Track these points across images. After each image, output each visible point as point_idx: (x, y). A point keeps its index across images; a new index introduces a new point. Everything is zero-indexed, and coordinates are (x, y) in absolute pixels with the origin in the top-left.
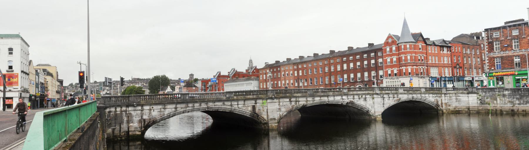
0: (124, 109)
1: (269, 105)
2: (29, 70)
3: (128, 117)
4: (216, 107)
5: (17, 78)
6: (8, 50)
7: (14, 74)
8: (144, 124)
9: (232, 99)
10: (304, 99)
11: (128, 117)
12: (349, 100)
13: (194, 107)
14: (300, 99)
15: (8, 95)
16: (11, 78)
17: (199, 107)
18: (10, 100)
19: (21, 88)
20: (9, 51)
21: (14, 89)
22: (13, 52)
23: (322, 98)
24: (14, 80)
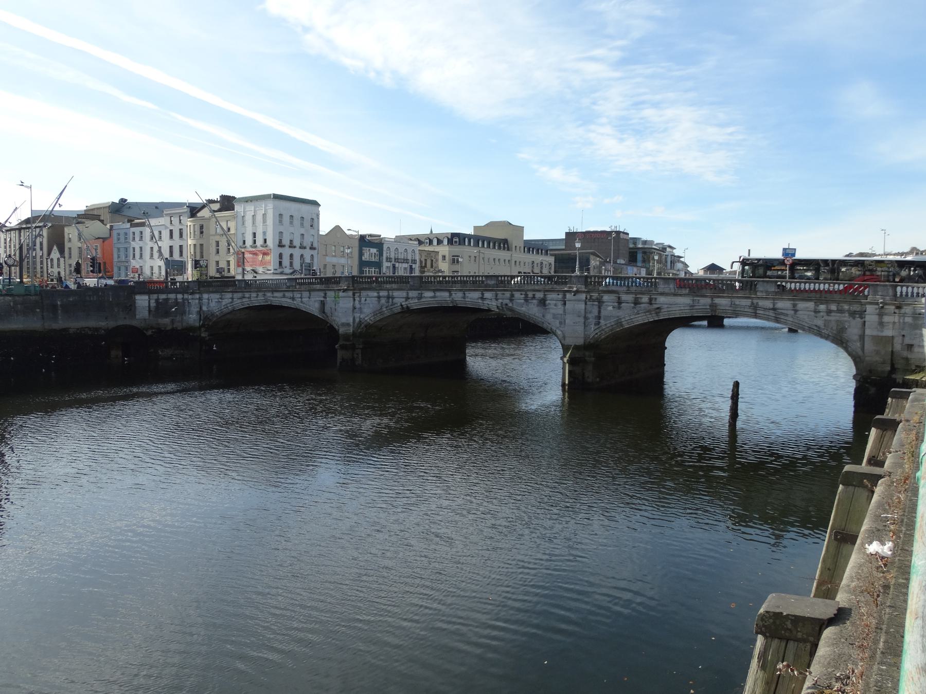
10: (404, 294)
14: (396, 294)
23: (438, 294)
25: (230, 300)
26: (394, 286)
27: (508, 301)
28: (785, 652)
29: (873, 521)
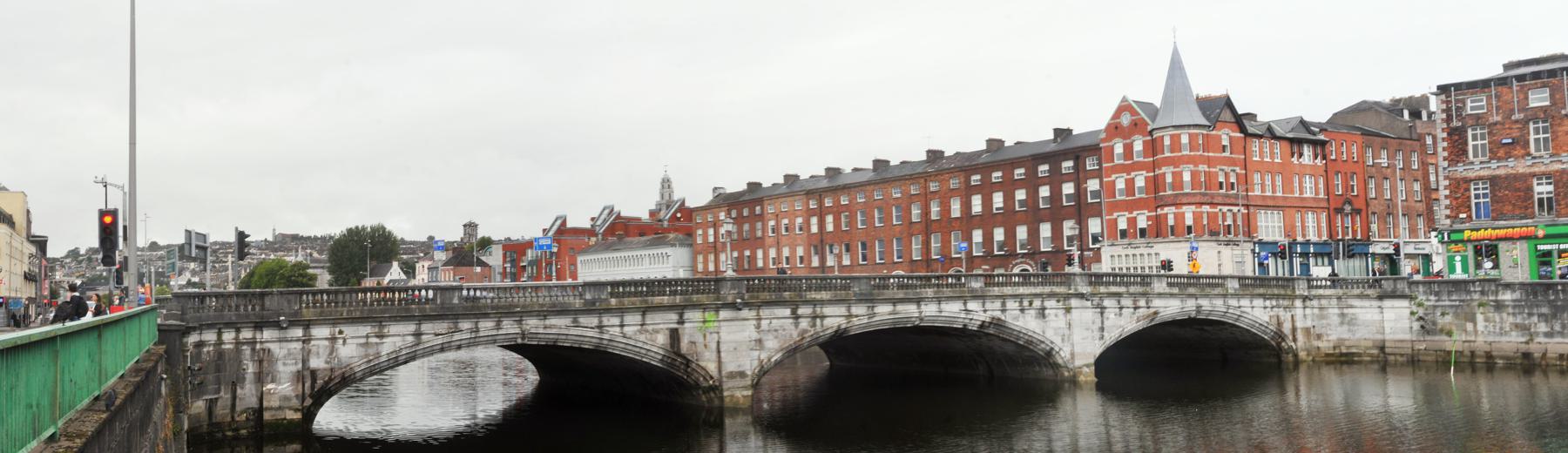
3: (261, 362)
8: (313, 387)
9: (604, 307)
10: (842, 310)
11: (261, 362)
13: (477, 331)
14: (828, 310)
17: (494, 332)
23: (900, 307)
25: (410, 339)
26: (825, 295)
27: (999, 313)
28: (836, 316)
29: (1102, 406)
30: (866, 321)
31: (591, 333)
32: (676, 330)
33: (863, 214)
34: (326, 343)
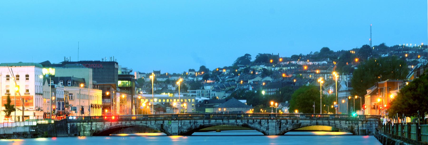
0: (82, 123)
1: (172, 124)
2: (43, 90)
3: (84, 128)
4: (136, 124)
5: (32, 100)
6: (25, 76)
7: (30, 96)
8: (93, 133)
9: (147, 119)
10: (202, 121)
11: (84, 128)
12: (243, 123)
13: (122, 123)
14: (198, 121)
15: (26, 114)
16: (28, 100)
17: (125, 124)
18: (27, 118)
19: (35, 108)
20: (26, 77)
21: (31, 108)
22: (29, 78)
23: (217, 121)
24: (30, 102)
30: (208, 123)
31: (144, 124)
32: (163, 124)
33: (414, 61)
34: (95, 125)
